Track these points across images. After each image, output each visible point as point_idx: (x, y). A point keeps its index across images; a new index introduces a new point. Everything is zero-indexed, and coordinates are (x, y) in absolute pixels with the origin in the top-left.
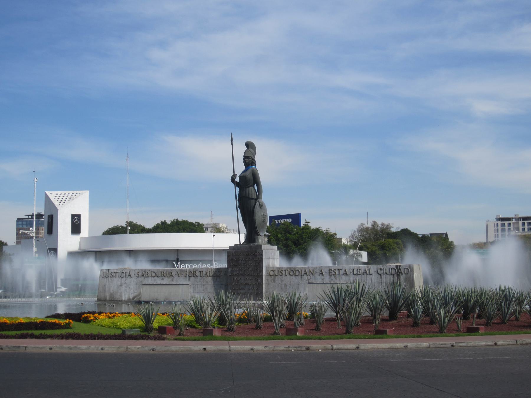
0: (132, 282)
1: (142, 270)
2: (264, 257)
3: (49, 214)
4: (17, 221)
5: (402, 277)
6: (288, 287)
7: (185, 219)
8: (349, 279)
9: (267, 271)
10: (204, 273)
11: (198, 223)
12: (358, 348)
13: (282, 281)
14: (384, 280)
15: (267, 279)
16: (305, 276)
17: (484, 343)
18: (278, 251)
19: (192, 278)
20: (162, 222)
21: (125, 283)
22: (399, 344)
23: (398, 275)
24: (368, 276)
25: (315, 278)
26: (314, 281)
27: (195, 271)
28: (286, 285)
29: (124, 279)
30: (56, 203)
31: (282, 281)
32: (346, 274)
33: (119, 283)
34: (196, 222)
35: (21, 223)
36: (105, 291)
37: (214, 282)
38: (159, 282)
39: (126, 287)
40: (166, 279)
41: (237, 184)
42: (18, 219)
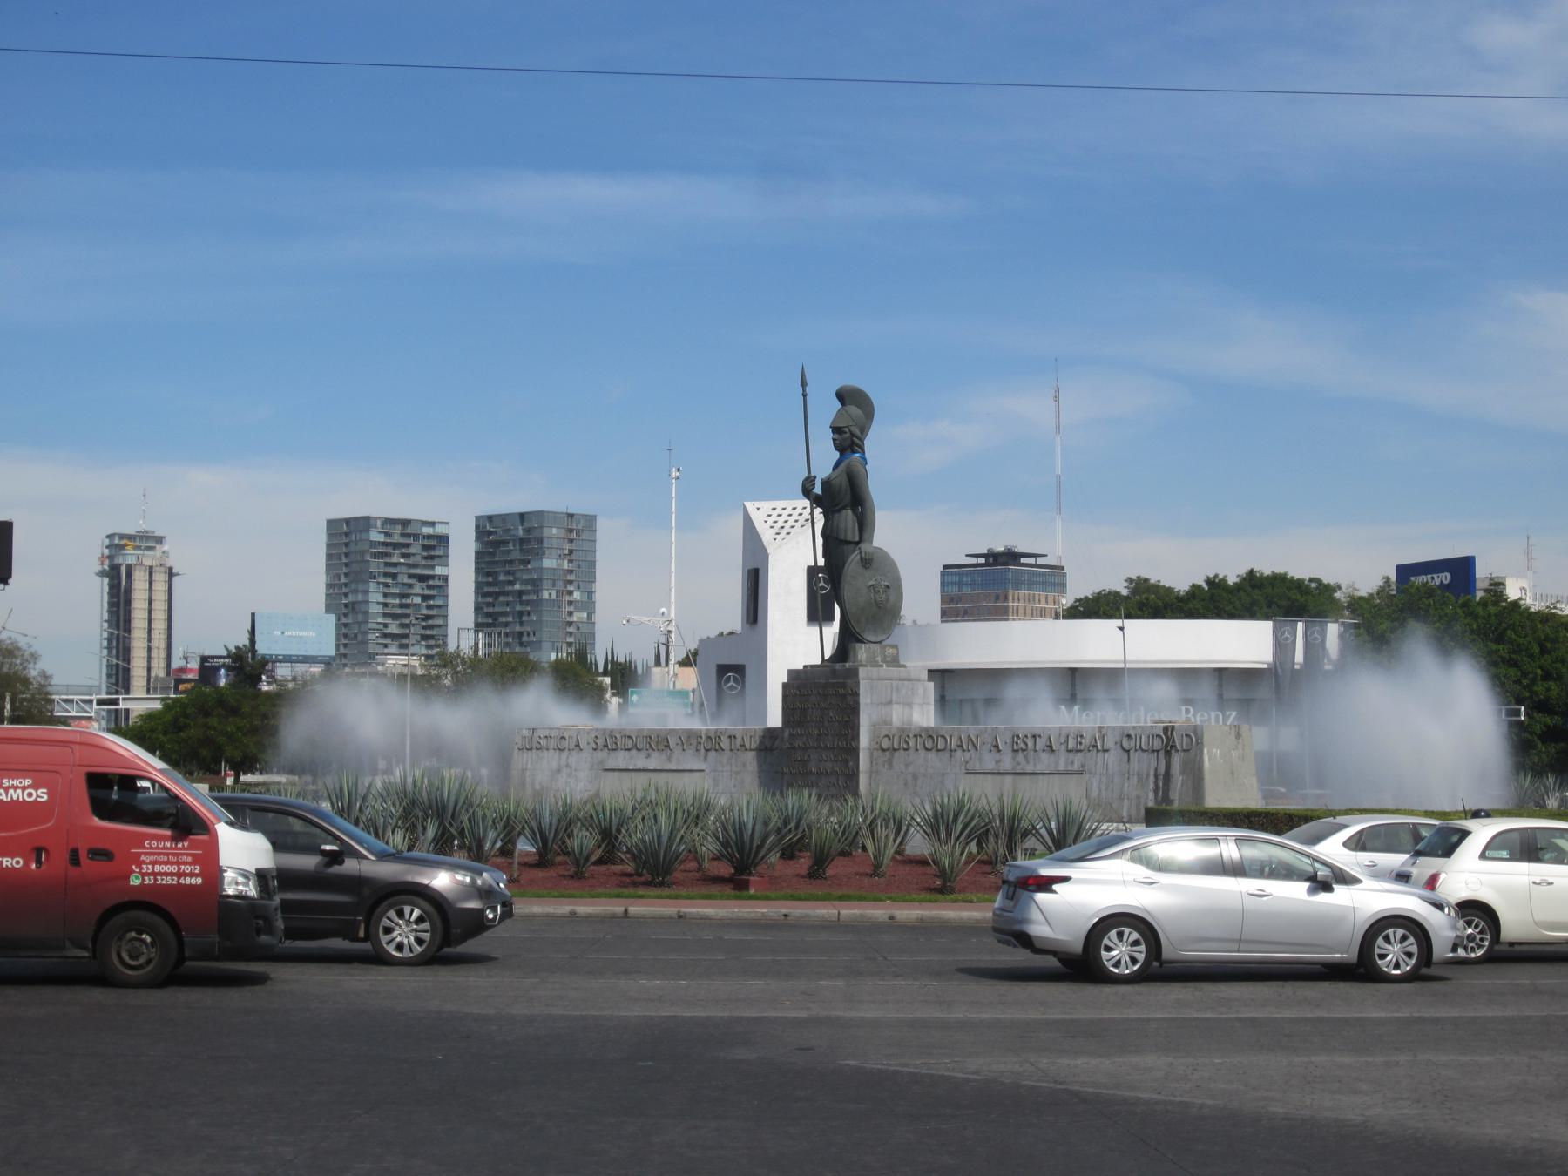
0: (582, 762)
1: (604, 731)
2: (865, 699)
3: (751, 566)
4: (943, 575)
5: (1177, 759)
6: (919, 782)
7: (1279, 570)
8: (1057, 763)
9: (875, 737)
10: (739, 741)
13: (907, 765)
14: (1135, 766)
15: (872, 760)
16: (959, 752)
18: (932, 684)
19: (713, 753)
20: (1209, 582)
21: (568, 766)
23: (1168, 754)
24: (1100, 755)
25: (980, 760)
26: (977, 768)
27: (718, 735)
28: (915, 777)
30: (766, 535)
31: (907, 765)
32: (1050, 748)
33: (554, 765)
34: (1311, 580)
36: (523, 784)
37: (760, 766)
38: (640, 765)
39: (569, 775)
40: (655, 755)
41: (817, 501)
42: (945, 567)
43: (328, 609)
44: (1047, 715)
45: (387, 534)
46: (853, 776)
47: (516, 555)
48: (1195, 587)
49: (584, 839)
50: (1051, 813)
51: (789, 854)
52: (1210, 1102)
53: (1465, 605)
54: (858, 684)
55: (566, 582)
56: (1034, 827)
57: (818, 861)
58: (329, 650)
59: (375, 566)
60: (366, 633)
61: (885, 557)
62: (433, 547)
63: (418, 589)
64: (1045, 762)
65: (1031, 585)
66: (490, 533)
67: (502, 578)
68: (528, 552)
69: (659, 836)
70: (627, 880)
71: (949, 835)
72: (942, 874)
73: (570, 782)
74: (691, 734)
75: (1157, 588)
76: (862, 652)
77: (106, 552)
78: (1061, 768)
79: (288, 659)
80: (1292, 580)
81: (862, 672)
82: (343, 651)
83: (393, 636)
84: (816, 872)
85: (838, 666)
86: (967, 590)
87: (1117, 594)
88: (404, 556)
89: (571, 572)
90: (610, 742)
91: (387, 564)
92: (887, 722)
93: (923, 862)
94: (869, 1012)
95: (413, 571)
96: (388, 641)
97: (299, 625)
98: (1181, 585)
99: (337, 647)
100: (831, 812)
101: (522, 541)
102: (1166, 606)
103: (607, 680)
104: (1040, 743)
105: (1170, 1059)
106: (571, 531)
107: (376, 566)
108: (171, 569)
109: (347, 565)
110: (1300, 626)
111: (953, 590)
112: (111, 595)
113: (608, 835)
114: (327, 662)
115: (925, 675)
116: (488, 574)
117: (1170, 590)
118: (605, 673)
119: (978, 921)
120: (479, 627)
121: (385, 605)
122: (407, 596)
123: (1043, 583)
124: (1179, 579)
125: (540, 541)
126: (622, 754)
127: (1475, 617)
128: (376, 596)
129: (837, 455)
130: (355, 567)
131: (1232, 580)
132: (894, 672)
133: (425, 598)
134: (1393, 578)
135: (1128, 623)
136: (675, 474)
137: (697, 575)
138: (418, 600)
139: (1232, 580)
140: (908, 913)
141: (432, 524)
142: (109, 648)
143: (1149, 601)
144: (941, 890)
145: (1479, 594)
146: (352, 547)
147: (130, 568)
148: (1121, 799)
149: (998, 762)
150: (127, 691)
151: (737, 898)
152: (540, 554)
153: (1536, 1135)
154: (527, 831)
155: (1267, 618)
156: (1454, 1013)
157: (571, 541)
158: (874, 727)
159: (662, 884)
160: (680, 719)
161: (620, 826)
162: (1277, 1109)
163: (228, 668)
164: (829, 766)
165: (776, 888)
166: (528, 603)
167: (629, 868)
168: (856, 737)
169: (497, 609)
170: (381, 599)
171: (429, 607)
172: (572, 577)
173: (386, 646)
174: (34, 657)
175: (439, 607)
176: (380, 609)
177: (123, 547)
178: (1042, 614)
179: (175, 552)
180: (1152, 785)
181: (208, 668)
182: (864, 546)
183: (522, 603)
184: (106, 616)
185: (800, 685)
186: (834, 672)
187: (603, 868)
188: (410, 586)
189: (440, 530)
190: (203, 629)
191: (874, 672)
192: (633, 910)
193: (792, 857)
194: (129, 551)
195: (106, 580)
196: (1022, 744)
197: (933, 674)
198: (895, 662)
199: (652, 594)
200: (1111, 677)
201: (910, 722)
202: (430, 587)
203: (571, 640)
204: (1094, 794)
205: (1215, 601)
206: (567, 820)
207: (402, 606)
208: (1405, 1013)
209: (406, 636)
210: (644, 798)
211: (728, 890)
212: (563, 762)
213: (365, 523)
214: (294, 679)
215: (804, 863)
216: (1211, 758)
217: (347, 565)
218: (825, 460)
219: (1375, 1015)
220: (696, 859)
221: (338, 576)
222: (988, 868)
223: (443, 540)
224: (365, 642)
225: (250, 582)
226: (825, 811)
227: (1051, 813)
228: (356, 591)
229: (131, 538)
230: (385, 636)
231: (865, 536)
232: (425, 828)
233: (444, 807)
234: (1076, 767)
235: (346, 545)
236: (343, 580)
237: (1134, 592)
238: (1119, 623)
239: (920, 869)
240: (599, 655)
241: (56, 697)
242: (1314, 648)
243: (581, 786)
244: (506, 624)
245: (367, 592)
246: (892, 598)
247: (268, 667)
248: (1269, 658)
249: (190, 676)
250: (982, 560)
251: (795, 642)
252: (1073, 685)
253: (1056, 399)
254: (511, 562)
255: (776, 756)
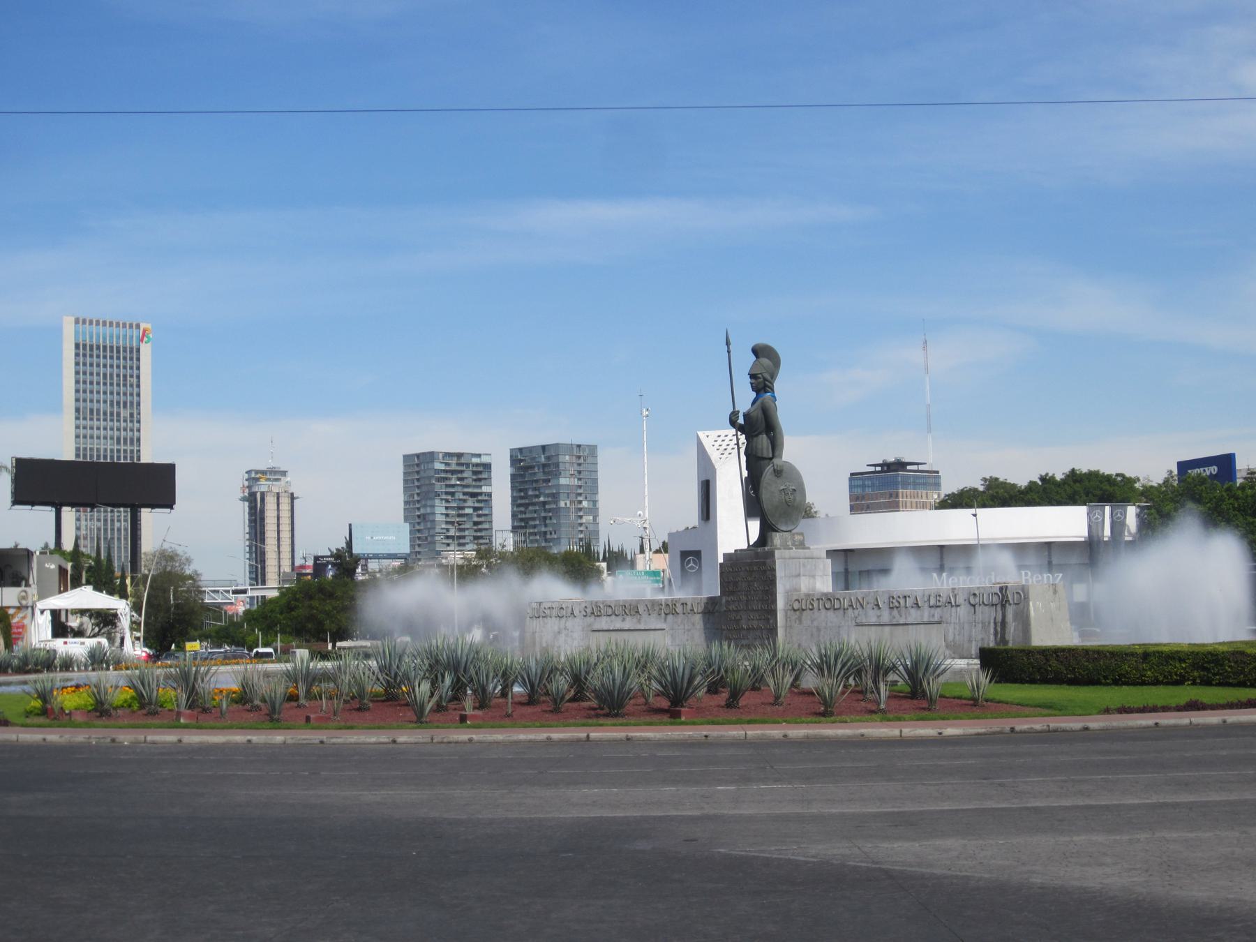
2: (779, 573)
4: (850, 480)
5: (1010, 611)
7: (1093, 469)
8: (922, 616)
10: (689, 607)
11: (1122, 475)
12: (180, 741)
14: (979, 616)
16: (850, 610)
17: (373, 740)
19: (670, 617)
20: (1043, 479)
22: (239, 738)
23: (1003, 606)
26: (864, 621)
27: (674, 602)
29: (563, 620)
30: (714, 455)
33: (556, 628)
34: (1117, 475)
35: (859, 483)
36: (534, 644)
37: (705, 625)
39: (567, 635)
40: (628, 619)
41: (741, 429)
43: (406, 519)
44: (905, 579)
45: (447, 464)
46: (773, 630)
47: (540, 476)
48: (1032, 483)
49: (561, 683)
50: (907, 655)
51: (713, 689)
52: (987, 876)
53: (1229, 489)
54: (774, 562)
55: (576, 493)
56: (894, 666)
57: (730, 694)
58: (405, 548)
59: (438, 485)
60: (433, 536)
61: (792, 468)
62: (480, 472)
63: (470, 503)
64: (914, 615)
65: (915, 485)
66: (521, 461)
67: (530, 493)
68: (549, 473)
69: (614, 680)
70: (592, 713)
71: (829, 672)
72: (825, 703)
73: (569, 642)
74: (654, 604)
75: (1004, 485)
76: (777, 539)
77: (246, 483)
78: (926, 619)
79: (376, 556)
80: (1103, 475)
81: (777, 553)
82: (417, 549)
83: (452, 537)
84: (732, 703)
85: (760, 550)
86: (869, 491)
87: (976, 490)
88: (459, 479)
89: (580, 487)
90: (595, 611)
91: (447, 486)
92: (797, 590)
93: (810, 693)
94: (746, 810)
95: (466, 490)
96: (450, 541)
97: (383, 530)
98: (1022, 481)
99: (412, 546)
100: (745, 658)
101: (544, 466)
102: (1011, 497)
103: (604, 565)
104: (910, 602)
105: (965, 842)
106: (579, 457)
107: (439, 487)
108: (292, 494)
109: (418, 487)
110: (1107, 509)
111: (858, 491)
112: (250, 514)
113: (578, 680)
114: (405, 557)
115: (824, 555)
116: (521, 490)
117: (1014, 486)
118: (604, 560)
119: (849, 737)
120: (515, 529)
121: (447, 515)
122: (463, 508)
123: (924, 484)
124: (1021, 478)
125: (557, 465)
126: (604, 619)
127: (1237, 499)
128: (440, 508)
129: (754, 395)
130: (424, 489)
131: (1059, 477)
132: (801, 552)
133: (475, 509)
134: (1175, 472)
135: (981, 511)
136: (645, 413)
137: (659, 489)
138: (469, 511)
139: (1059, 477)
140: (798, 732)
141: (479, 456)
142: (250, 552)
143: (1000, 495)
144: (823, 714)
145: (1239, 481)
146: (422, 474)
147: (263, 494)
148: (970, 641)
149: (879, 617)
150: (264, 582)
151: (672, 724)
152: (557, 475)
153: (1231, 896)
154: (520, 679)
155: (1085, 504)
156: (1191, 798)
157: (579, 465)
158: (788, 594)
159: (617, 715)
160: (648, 591)
161: (588, 673)
162: (1037, 880)
163: (334, 565)
164: (755, 624)
165: (703, 716)
166: (550, 510)
167: (594, 703)
168: (774, 601)
169: (528, 516)
170: (444, 511)
171: (479, 516)
172: (581, 491)
173: (448, 545)
174: (189, 561)
175: (485, 515)
176: (443, 518)
177: (258, 479)
178: (924, 506)
179: (294, 482)
180: (992, 631)
181: (319, 566)
182: (776, 461)
183: (545, 510)
184: (247, 530)
185: (734, 562)
186: (757, 554)
187: (575, 705)
188: (465, 501)
189: (484, 460)
190: (316, 538)
191: (787, 553)
192: (593, 735)
193: (716, 692)
194: (263, 482)
195: (247, 504)
196: (895, 603)
197: (831, 553)
198: (801, 545)
199: (637, 502)
200: (966, 551)
201: (814, 589)
202: (479, 501)
203: (581, 536)
204: (950, 637)
205: (1046, 492)
206: (549, 670)
207: (459, 515)
208: (1154, 799)
209: (464, 537)
210: (606, 651)
211: (666, 718)
212: (562, 626)
213: (431, 456)
214: (380, 571)
215: (724, 695)
216: (1035, 609)
217: (418, 487)
218: (745, 399)
219: (1131, 802)
220: (644, 696)
221: (412, 495)
222: (860, 697)
223: (487, 467)
224: (434, 543)
225: (349, 501)
226: (741, 657)
227: (907, 655)
228: (425, 506)
229: (263, 472)
230: (448, 537)
231: (777, 453)
232: (443, 677)
233: (459, 663)
234: (936, 619)
235: (418, 473)
236: (416, 498)
237: (988, 488)
238: (972, 511)
239: (810, 699)
240: (600, 548)
241: (207, 589)
242: (1118, 526)
243: (576, 643)
244: (535, 527)
245: (433, 506)
246: (798, 499)
247: (362, 562)
248: (1086, 534)
249: (308, 571)
250: (879, 469)
251: (734, 531)
252: (942, 558)
253: (925, 348)
254: (537, 481)
255: (717, 617)
